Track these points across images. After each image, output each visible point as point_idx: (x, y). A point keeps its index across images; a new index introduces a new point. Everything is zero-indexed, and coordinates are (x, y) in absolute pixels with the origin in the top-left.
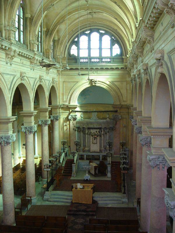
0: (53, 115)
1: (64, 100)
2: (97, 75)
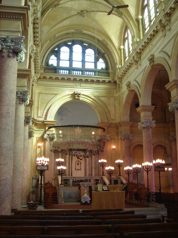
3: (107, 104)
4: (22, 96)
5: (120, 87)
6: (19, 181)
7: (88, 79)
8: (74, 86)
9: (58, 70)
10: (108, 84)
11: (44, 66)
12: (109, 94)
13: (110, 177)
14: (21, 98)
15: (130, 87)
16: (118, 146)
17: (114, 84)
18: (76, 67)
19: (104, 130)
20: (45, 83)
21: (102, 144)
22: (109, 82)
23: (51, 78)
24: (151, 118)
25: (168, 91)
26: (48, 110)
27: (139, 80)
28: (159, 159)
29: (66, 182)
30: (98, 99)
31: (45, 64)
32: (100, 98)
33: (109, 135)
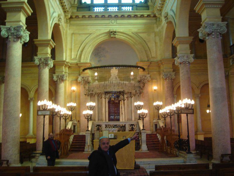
0: (57, 74)
1: (73, 57)
2: (117, 24)
3: (146, 41)
4: (16, 32)
5: (161, 20)
6: (13, 128)
7: (124, 15)
8: (109, 23)
9: (91, 8)
10: (147, 18)
11: (76, 4)
12: (148, 29)
13: (165, 120)
14: (15, 34)
15: (167, 19)
16: (160, 87)
17: (154, 18)
18: (114, 3)
19: (144, 69)
20: (78, 22)
21: (142, 85)
22: (148, 16)
23: (84, 17)
24: (189, 51)
25: (198, 14)
26: (82, 51)
27: (174, 9)
28: (186, 99)
29: (132, 127)
30: (137, 36)
31: (78, 3)
32: (139, 34)
33: (149, 75)
